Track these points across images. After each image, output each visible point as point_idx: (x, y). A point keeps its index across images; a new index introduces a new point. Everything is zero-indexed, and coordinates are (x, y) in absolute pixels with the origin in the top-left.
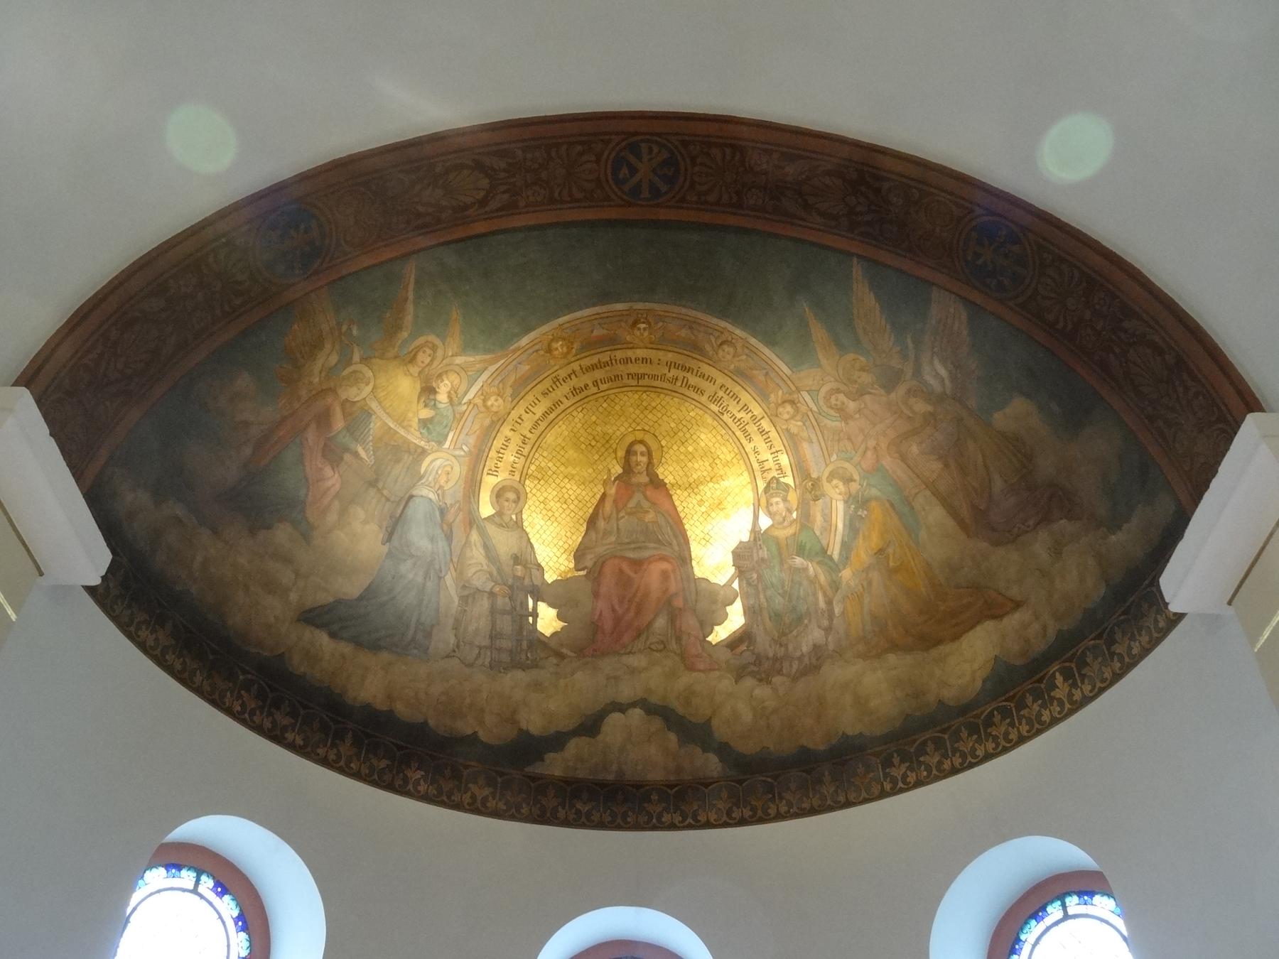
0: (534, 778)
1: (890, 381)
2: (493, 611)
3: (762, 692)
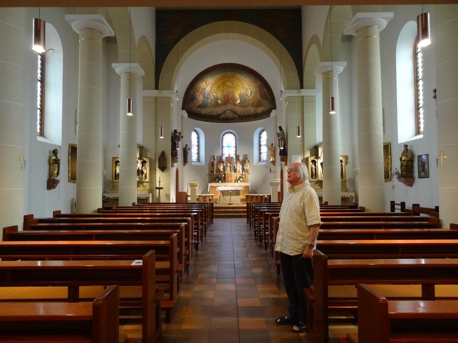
2: (214, 102)
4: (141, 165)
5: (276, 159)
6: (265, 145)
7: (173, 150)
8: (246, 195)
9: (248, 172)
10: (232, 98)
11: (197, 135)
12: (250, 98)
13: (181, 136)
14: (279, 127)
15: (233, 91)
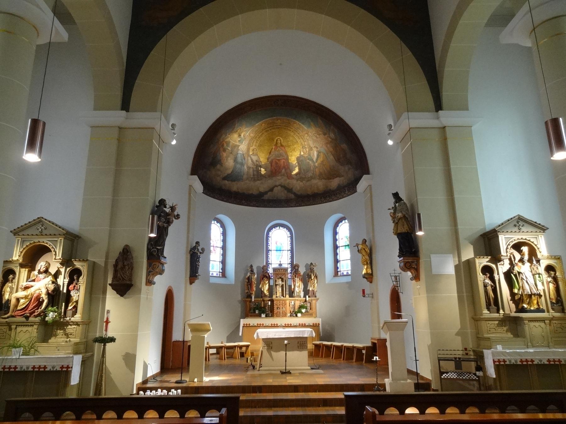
0: (263, 200)
1: (325, 134)
2: (253, 171)
3: (301, 183)
4: (67, 280)
5: (374, 268)
6: (345, 246)
7: (152, 244)
8: (314, 342)
9: (316, 297)
10: (285, 164)
11: (221, 229)
12: (316, 164)
13: (176, 213)
14: (393, 194)
15: (286, 153)
